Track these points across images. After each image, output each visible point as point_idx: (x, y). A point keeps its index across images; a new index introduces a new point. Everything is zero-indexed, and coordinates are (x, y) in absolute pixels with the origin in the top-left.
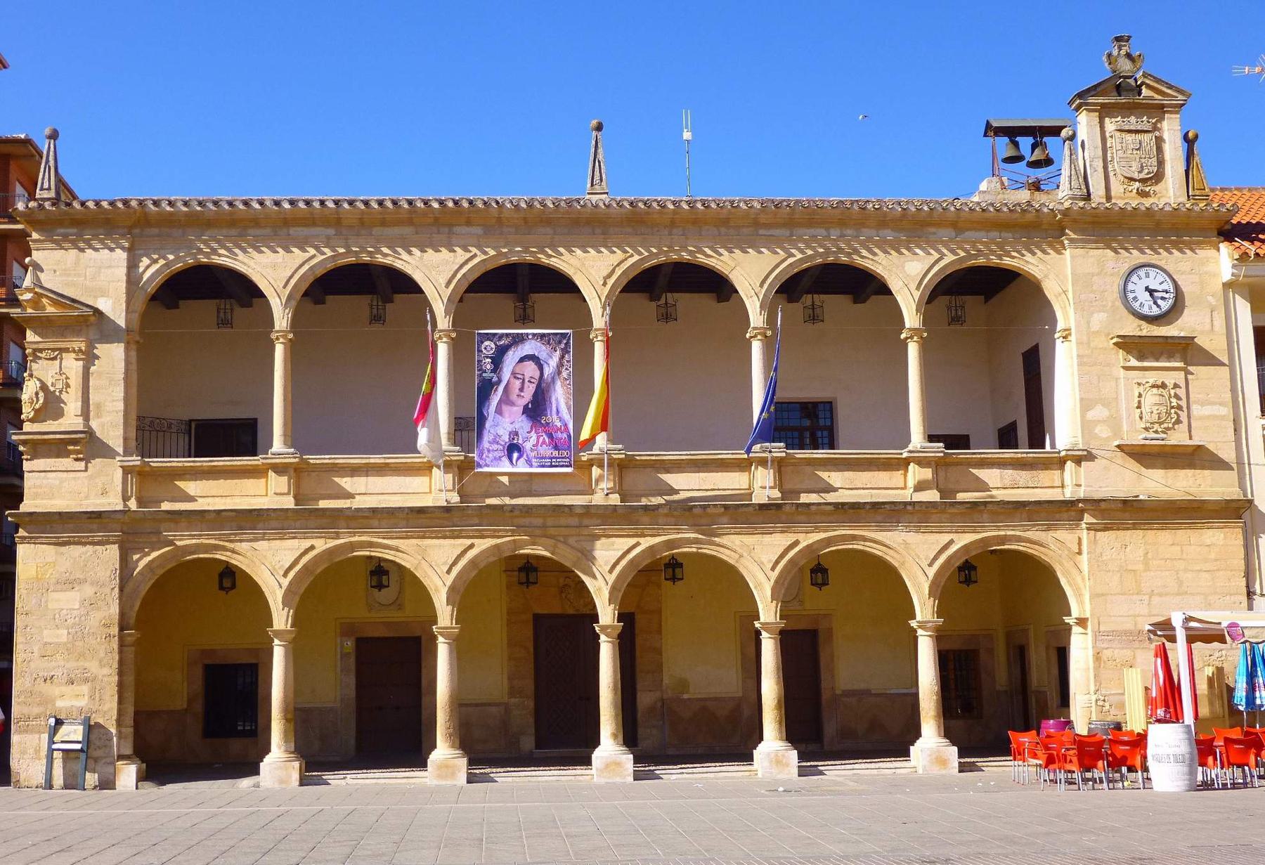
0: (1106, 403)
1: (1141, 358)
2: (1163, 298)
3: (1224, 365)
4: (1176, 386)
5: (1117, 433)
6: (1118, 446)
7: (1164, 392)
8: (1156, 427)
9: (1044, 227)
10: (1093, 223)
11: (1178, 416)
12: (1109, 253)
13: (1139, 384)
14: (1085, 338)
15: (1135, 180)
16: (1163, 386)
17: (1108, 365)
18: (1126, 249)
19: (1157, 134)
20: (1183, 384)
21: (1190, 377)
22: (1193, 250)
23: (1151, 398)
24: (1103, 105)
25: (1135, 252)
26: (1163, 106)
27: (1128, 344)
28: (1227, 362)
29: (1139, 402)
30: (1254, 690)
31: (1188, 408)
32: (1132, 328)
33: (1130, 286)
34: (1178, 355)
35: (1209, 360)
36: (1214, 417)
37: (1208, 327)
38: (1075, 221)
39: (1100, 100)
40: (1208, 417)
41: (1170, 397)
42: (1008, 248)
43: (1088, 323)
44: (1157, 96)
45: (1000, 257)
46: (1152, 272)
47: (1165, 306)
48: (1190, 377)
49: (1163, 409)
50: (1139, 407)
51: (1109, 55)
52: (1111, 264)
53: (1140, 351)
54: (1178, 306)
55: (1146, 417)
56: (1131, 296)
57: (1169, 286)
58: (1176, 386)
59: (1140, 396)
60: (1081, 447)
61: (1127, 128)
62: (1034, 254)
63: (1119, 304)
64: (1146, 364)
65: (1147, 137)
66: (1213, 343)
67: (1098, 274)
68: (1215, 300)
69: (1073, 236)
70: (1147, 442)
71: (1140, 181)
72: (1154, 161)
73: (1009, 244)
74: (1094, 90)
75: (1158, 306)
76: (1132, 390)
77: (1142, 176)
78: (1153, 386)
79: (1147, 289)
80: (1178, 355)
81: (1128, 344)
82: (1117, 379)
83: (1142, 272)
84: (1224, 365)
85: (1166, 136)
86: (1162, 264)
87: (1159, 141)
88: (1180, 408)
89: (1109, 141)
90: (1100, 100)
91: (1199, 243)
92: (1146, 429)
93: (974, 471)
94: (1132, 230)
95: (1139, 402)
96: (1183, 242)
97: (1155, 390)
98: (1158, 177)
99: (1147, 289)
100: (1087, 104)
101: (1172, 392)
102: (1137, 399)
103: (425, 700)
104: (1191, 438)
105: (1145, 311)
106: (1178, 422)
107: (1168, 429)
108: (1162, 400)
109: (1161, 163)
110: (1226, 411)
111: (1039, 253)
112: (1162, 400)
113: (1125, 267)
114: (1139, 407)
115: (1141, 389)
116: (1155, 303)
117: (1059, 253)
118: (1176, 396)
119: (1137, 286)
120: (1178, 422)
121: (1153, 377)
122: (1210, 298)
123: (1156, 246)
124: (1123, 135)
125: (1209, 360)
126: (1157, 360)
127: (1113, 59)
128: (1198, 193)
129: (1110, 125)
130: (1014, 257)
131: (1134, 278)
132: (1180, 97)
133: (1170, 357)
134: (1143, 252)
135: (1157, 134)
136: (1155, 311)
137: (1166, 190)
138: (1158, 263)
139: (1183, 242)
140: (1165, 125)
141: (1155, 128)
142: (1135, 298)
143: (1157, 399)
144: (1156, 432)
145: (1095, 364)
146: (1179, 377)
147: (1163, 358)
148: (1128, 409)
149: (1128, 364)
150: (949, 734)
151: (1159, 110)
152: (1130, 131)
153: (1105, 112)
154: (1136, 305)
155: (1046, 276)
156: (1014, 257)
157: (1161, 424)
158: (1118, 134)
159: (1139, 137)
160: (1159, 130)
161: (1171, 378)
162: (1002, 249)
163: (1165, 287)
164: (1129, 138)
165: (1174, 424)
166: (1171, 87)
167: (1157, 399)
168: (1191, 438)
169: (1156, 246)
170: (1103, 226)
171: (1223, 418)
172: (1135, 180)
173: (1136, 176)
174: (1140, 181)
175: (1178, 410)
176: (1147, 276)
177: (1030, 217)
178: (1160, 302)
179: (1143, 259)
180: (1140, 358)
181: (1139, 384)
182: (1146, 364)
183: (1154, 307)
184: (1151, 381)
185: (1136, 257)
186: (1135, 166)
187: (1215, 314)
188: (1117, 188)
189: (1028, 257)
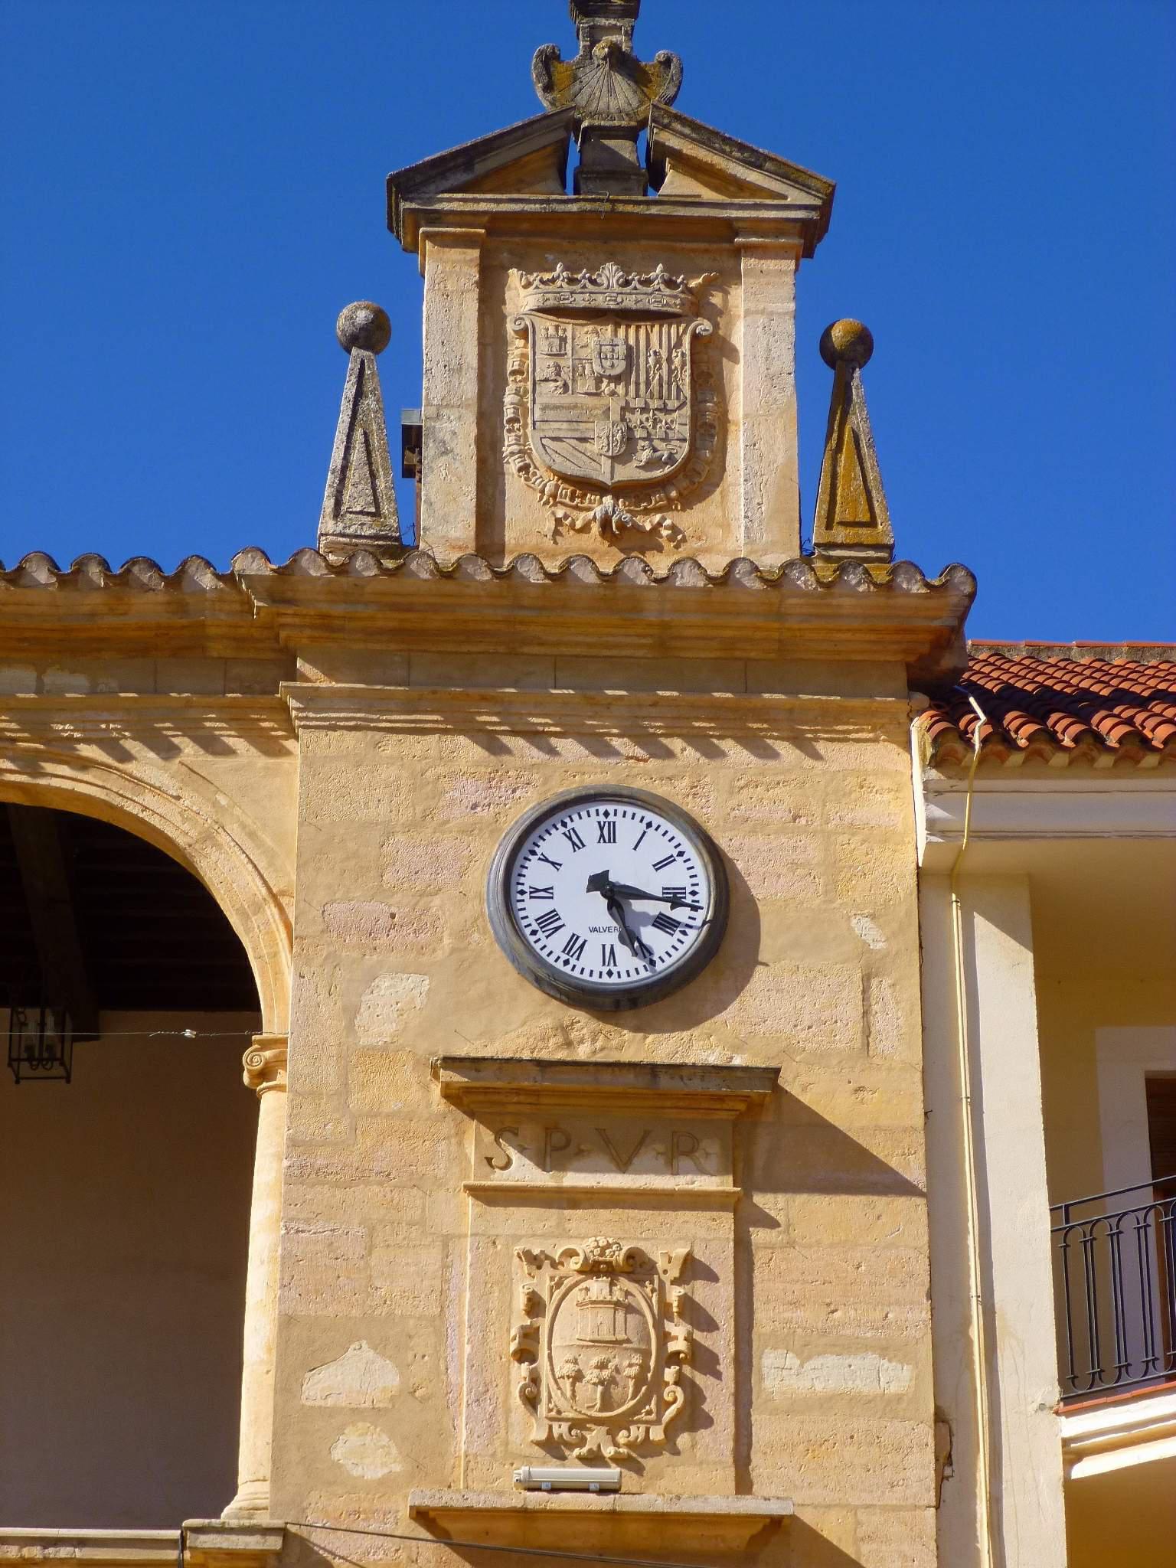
0: (390, 1341)
1: (554, 1151)
2: (663, 923)
3: (905, 1188)
4: (692, 1269)
5: (424, 1450)
6: (422, 1516)
7: (640, 1295)
8: (595, 1437)
9: (216, 649)
10: (398, 633)
11: (694, 1396)
12: (467, 750)
13: (535, 1261)
14: (330, 1073)
15: (601, 489)
16: (637, 1267)
17: (416, 1183)
18: (534, 736)
19: (704, 326)
20: (723, 1261)
21: (759, 1236)
22: (799, 741)
23: (578, 1324)
24: (497, 224)
25: (569, 748)
26: (730, 229)
27: (493, 1095)
28: (915, 1172)
29: (529, 1335)
31: (744, 1362)
32: (524, 1028)
33: (534, 874)
34: (712, 1147)
35: (844, 1166)
36: (856, 1403)
37: (848, 1034)
38: (326, 625)
39: (486, 203)
40: (826, 1403)
42: (64, 729)
43: (351, 1012)
44: (708, 195)
45: (30, 763)
46: (628, 822)
47: (670, 950)
48: (759, 1236)
49: (628, 1365)
50: (526, 1353)
51: (549, 60)
52: (472, 790)
53: (549, 1130)
54: (727, 945)
56: (532, 910)
57: (691, 874)
58: (692, 1269)
59: (535, 1306)
60: (264, 1520)
61: (580, 301)
62: (168, 751)
63: (486, 942)
64: (573, 1179)
65: (658, 337)
66: (867, 1099)
67: (410, 827)
68: (887, 936)
69: (324, 683)
70: (536, 1500)
71: (620, 490)
72: (681, 423)
73: (66, 710)
74: (466, 166)
75: (644, 951)
76: (507, 1285)
77: (629, 472)
78: (592, 1269)
79: (599, 882)
80: (712, 1147)
81: (493, 1095)
82: (447, 1242)
83: (586, 824)
84: (905, 1188)
85: (739, 337)
86: (675, 792)
87: (709, 361)
88: (701, 1358)
89: (516, 349)
90: (486, 203)
91: (831, 721)
92: (553, 1447)
94: (563, 665)
95: (529, 1335)
96: (762, 713)
97: (598, 1287)
98: (695, 477)
99: (599, 882)
100: (436, 218)
101: (674, 1294)
103: (691, 1539)
104: (743, 1484)
105: (589, 968)
106: (694, 1417)
108: (626, 1327)
109: (709, 428)
110: (905, 1378)
111: (189, 749)
112: (626, 1327)
113: (528, 803)
114: (526, 1353)
115: (542, 1282)
116: (630, 937)
117: (272, 748)
118: (691, 1311)
119: (562, 875)
120: (694, 1417)
121: (590, 1234)
122: (865, 929)
123: (656, 726)
124: (569, 327)
125: (844, 1166)
127: (560, 71)
128: (840, 535)
129: (522, 295)
130: (85, 764)
131: (554, 844)
132: (795, 196)
133: (679, 1151)
134: (599, 747)
135: (704, 326)
136: (629, 970)
137: (726, 526)
138: (661, 790)
139: (762, 713)
140: (739, 298)
141: (697, 305)
142: (550, 921)
144: (594, 1459)
145: (361, 1177)
146: (711, 1236)
147: (646, 1157)
148: (478, 1366)
149: (500, 1178)
151: (714, 246)
152: (594, 315)
153: (501, 247)
154: (553, 946)
155: (208, 837)
156: (85, 764)
157: (614, 1426)
158: (546, 325)
159: (628, 334)
160: (716, 315)
161: (666, 1240)
162: (39, 730)
163: (676, 876)
164: (588, 338)
166: (756, 161)
168: (743, 1484)
169: (656, 726)
170: (457, 648)
171: (889, 1405)
172: (601, 489)
173: (603, 472)
174: (620, 490)
175: (693, 1369)
176: (608, 834)
177: (149, 605)
178: (650, 935)
179: (598, 773)
180: (550, 1156)
181: (535, 1261)
182: (573, 1179)
183: (623, 952)
184: (586, 1247)
185: (574, 765)
186: (602, 435)
187: (881, 988)
188: (527, 518)
189: (146, 763)
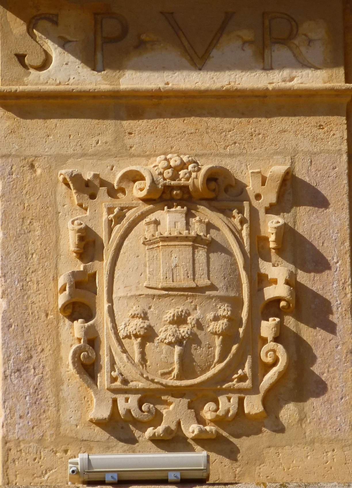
4: (293, 192)
7: (225, 228)
8: (173, 412)
13: (87, 188)
16: (221, 191)
23: (144, 269)
30: (113, 327)
34: (315, 31)
41: (258, 249)
49: (213, 319)
50: (79, 308)
55: (118, 359)
58: (293, 192)
59: (89, 245)
64: (134, 80)
78: (163, 196)
80: (315, 31)
92: (119, 428)
93: (131, 426)
97: (170, 220)
101: (270, 225)
102: (70, 265)
107: (240, 423)
108: (209, 269)
114: (79, 308)
115: (98, 216)
118: (296, 248)
121: (158, 151)
126: (199, 61)
143: (175, 264)
147: (229, 47)
149: (35, 81)
150: (137, 429)
157: (196, 397)
165: (273, 400)
167: (175, 264)
180: (104, 48)
181: (87, 188)
182: (134, 80)
184: (153, 168)
